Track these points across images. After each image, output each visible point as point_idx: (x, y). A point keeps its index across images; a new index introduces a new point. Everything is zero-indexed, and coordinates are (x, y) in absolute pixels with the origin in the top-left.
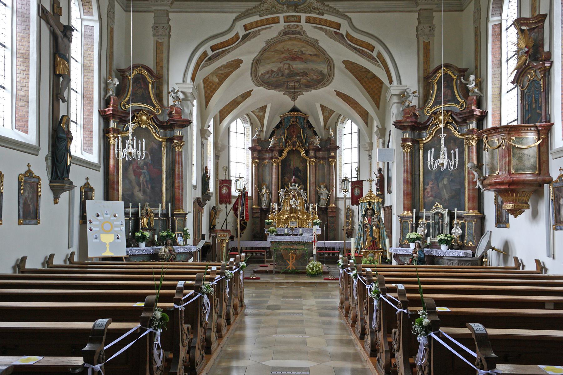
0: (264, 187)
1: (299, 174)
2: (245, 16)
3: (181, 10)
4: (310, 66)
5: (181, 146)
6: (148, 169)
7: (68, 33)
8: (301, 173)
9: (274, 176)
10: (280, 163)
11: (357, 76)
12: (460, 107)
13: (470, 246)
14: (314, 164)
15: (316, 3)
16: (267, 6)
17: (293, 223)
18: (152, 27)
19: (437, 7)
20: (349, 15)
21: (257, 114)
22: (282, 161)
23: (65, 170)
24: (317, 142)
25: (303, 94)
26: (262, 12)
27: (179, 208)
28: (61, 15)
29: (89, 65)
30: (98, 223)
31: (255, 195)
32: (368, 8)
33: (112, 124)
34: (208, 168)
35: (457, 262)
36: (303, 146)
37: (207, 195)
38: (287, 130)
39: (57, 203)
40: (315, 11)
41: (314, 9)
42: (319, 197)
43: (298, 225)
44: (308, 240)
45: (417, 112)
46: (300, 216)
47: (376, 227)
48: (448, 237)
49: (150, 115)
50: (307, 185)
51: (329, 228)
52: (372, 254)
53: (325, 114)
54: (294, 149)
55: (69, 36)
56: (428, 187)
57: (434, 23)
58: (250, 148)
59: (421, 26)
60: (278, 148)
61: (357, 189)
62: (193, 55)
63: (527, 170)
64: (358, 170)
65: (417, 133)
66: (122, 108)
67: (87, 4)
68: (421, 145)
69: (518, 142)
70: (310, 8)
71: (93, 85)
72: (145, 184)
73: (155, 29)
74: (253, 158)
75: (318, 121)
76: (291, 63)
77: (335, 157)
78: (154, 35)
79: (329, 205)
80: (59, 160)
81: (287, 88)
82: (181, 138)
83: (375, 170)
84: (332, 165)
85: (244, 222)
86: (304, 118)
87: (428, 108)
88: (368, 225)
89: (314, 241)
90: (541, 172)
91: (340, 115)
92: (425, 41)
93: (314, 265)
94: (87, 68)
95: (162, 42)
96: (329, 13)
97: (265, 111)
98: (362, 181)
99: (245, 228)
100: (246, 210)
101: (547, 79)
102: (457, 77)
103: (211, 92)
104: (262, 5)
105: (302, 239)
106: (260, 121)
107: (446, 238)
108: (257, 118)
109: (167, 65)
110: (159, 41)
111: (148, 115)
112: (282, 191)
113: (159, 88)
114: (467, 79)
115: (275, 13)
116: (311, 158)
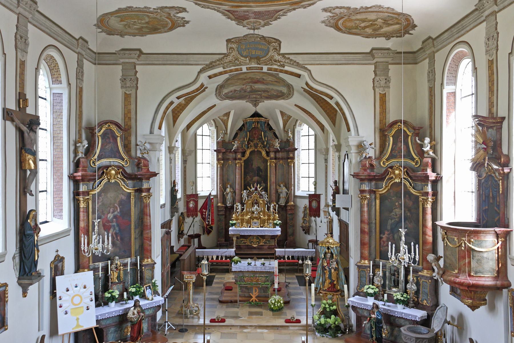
0: (229, 186)
1: (261, 173)
2: (209, 68)
3: (147, 62)
4: (271, 87)
5: (149, 198)
6: (117, 222)
7: (34, 127)
8: (262, 172)
9: (237, 176)
10: (243, 164)
11: (315, 98)
12: (415, 164)
13: (424, 304)
14: (274, 165)
15: (277, 56)
16: (231, 58)
17: (255, 223)
18: (120, 80)
19: (392, 60)
20: (309, 67)
21: (222, 118)
22: (245, 161)
23: (33, 265)
24: (277, 145)
25: (264, 102)
26: (225, 64)
27: (148, 258)
28: (28, 107)
29: (59, 132)
30: (68, 298)
31: (220, 194)
32: (326, 61)
33: (83, 188)
34: (176, 181)
35: (414, 339)
36: (264, 147)
37: (175, 207)
38: (249, 132)
39: (25, 296)
40: (276, 63)
41: (276, 61)
42: (279, 195)
43: (260, 225)
44: (269, 270)
45: (374, 163)
46: (262, 216)
47: (335, 270)
48: (404, 297)
49: (118, 170)
50: (267, 184)
51: (288, 225)
52: (331, 296)
53: (284, 118)
54: (256, 150)
55: (35, 130)
56: (384, 236)
57: (389, 75)
58: (215, 151)
59: (377, 78)
60: (241, 150)
61: (314, 202)
62: (160, 107)
63: (485, 273)
64: (315, 184)
65: (373, 183)
66: (92, 164)
67: (56, 73)
68: (378, 196)
69: (477, 244)
70: (272, 61)
71: (62, 151)
72: (114, 236)
73: (123, 81)
74: (218, 160)
75: (277, 123)
76: (253, 85)
77: (293, 158)
78: (122, 87)
79: (288, 203)
80: (27, 256)
81: (249, 98)
82: (148, 190)
83: (331, 183)
84: (291, 166)
85: (209, 226)
86: (265, 122)
87: (384, 160)
88: (327, 268)
89: (276, 276)
90: (500, 275)
91: (297, 120)
92: (381, 93)
93: (275, 301)
94: (56, 136)
95: (130, 94)
96: (290, 65)
97: (229, 116)
98: (320, 195)
99: (211, 231)
100: (212, 215)
101: (505, 182)
102: (412, 134)
103: (178, 112)
104: (225, 58)
105: (265, 269)
106: (224, 124)
107: (402, 298)
108: (222, 121)
109: (135, 116)
110: (127, 93)
111: (117, 170)
112: (245, 193)
113: (127, 140)
114: (422, 140)
115: (238, 65)
116: (271, 159)
